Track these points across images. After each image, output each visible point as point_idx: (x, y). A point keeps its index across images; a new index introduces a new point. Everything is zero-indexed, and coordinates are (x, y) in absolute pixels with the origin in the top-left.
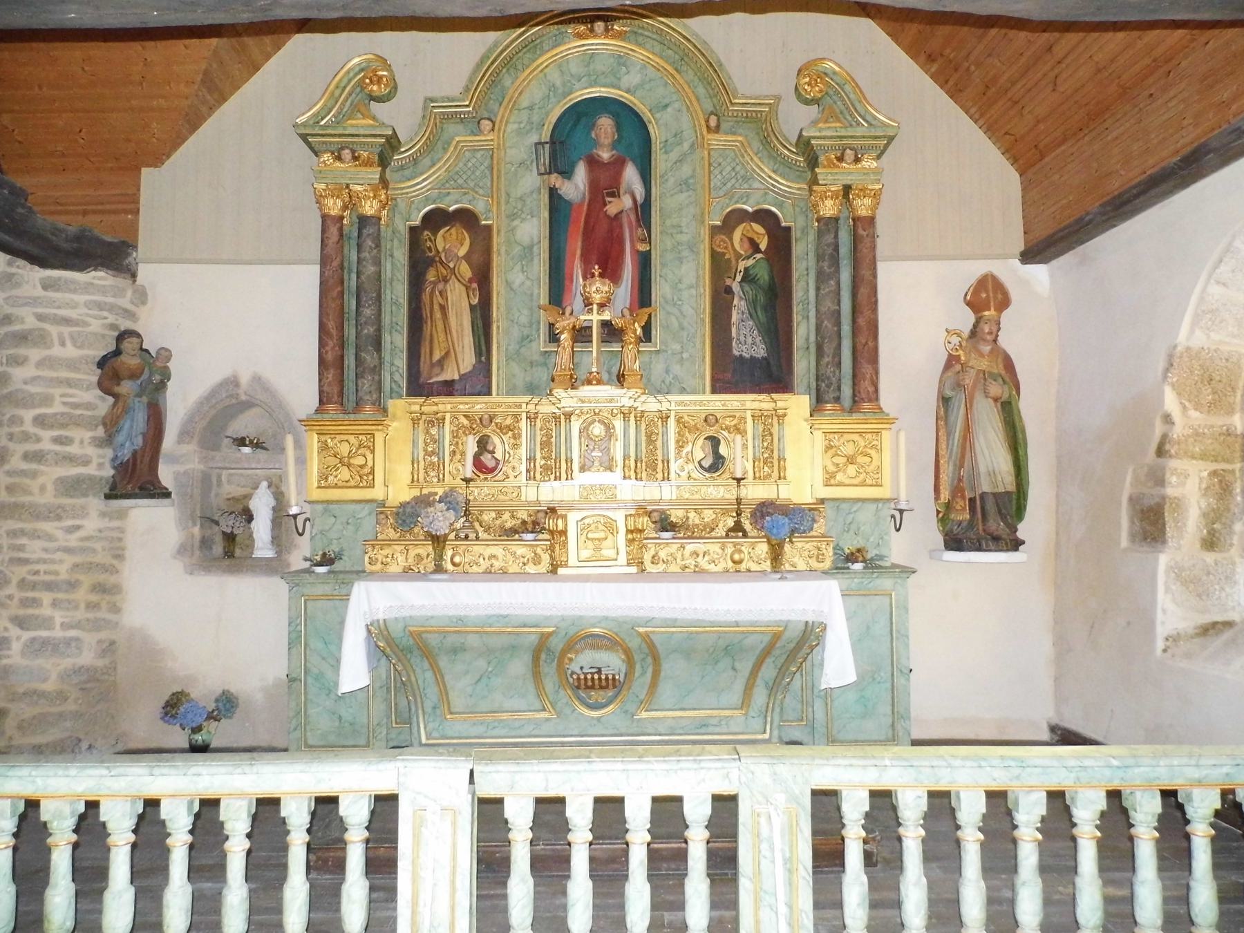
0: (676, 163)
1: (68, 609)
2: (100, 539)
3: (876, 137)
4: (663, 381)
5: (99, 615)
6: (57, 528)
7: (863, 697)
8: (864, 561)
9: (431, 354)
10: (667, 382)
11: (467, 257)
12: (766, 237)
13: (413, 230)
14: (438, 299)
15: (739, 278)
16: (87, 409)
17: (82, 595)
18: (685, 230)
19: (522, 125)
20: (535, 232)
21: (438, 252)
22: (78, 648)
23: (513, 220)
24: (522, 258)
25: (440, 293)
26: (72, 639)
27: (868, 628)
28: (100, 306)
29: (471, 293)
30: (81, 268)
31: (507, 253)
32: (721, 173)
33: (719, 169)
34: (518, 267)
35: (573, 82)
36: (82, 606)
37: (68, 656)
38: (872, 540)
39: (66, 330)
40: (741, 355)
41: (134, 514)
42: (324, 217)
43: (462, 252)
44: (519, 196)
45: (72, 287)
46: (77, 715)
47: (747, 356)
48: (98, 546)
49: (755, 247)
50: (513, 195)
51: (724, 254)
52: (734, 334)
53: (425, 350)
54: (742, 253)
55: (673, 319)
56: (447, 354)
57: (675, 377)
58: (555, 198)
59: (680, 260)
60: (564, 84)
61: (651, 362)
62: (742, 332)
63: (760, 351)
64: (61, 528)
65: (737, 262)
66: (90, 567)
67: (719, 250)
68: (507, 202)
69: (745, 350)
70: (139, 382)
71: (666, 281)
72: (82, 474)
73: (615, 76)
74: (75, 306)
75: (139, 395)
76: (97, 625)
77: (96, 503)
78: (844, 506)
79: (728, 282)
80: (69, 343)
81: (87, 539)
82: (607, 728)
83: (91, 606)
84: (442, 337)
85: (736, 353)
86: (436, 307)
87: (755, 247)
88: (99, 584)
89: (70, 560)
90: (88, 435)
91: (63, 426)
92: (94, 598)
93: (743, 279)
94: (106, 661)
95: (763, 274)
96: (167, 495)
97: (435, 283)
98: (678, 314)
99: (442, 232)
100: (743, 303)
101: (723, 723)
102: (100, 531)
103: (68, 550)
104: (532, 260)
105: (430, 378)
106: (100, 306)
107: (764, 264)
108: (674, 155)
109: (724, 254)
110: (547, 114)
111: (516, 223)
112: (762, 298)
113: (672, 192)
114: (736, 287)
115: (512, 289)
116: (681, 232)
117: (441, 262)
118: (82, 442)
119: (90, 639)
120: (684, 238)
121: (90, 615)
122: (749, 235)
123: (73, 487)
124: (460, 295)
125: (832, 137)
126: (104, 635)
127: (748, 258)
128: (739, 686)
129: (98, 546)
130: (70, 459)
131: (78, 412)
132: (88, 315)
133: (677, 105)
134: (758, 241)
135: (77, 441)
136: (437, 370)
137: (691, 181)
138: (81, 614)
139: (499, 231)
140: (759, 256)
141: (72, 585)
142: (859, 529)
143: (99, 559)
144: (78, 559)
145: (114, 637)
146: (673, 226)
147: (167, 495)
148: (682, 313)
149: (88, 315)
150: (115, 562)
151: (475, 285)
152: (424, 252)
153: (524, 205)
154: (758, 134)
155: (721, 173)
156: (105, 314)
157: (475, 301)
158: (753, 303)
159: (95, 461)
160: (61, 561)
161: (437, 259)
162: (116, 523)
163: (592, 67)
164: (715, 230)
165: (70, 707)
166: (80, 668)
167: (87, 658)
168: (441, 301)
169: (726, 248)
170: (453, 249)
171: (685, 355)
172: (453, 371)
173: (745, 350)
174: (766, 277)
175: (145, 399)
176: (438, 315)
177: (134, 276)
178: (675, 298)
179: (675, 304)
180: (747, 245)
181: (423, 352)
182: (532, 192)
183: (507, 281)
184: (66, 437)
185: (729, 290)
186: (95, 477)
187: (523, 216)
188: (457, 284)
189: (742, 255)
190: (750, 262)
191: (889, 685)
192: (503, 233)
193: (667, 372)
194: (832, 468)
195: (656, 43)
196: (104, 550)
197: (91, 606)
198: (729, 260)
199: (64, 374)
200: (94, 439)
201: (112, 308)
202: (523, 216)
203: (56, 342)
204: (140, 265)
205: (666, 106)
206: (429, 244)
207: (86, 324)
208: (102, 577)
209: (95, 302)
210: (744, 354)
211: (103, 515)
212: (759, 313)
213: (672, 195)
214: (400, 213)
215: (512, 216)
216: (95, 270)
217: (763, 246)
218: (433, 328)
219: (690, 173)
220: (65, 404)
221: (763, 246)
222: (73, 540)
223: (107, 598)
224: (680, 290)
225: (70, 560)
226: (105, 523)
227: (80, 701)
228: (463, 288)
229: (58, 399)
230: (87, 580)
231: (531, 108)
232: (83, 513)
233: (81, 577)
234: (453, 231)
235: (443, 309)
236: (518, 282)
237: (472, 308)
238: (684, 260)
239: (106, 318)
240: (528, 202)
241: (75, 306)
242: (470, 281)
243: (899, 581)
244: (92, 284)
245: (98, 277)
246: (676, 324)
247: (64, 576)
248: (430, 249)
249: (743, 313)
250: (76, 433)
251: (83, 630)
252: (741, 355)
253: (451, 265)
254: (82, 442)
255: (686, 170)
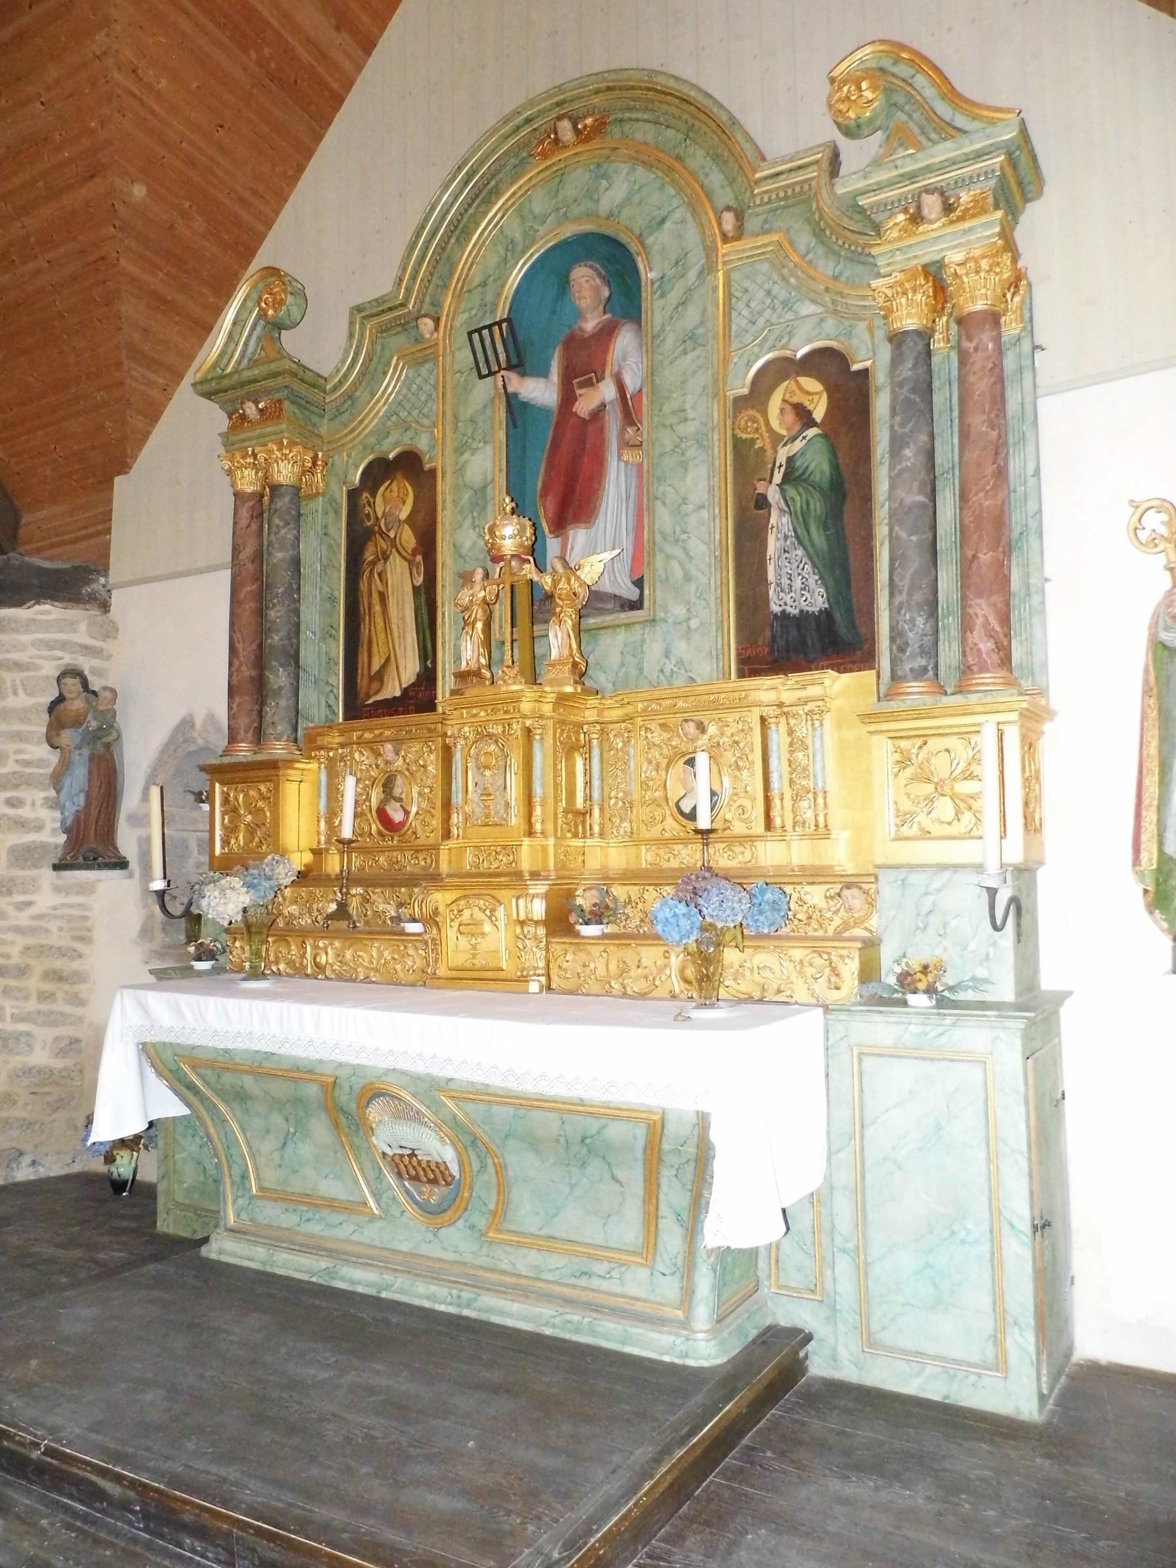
0: (677, 307)
1: (17, 999)
2: (55, 917)
3: (979, 155)
4: (662, 671)
5: (53, 1007)
6: (8, 904)
7: (929, 1266)
8: (930, 990)
9: (370, 662)
10: (667, 672)
11: (410, 520)
12: (825, 396)
13: (353, 495)
14: (377, 584)
15: (778, 477)
16: (38, 766)
17: (33, 983)
18: (691, 415)
19: (474, 312)
20: (489, 465)
21: (377, 519)
22: (28, 1045)
23: (462, 453)
24: (473, 505)
25: (379, 575)
26: (21, 1033)
27: (939, 1128)
28: (48, 645)
29: (415, 570)
30: (19, 604)
31: (455, 503)
32: (748, 306)
33: (746, 298)
34: (468, 522)
35: (536, 227)
36: (34, 996)
37: (17, 1054)
38: (972, 946)
39: (19, 676)
40: (784, 611)
41: (101, 888)
42: (238, 496)
43: (404, 513)
44: (469, 416)
45: (13, 625)
46: (27, 1124)
47: (795, 612)
48: (53, 926)
49: (804, 416)
50: (462, 417)
51: (753, 441)
52: (771, 576)
53: (363, 658)
54: (784, 432)
55: (675, 565)
56: (388, 660)
57: (680, 663)
58: (516, 409)
59: (684, 466)
60: (525, 234)
61: (643, 641)
62: (785, 570)
63: (816, 600)
64: (13, 904)
65: (776, 452)
66: (42, 951)
67: (744, 436)
68: (456, 429)
69: (789, 602)
70: (80, 730)
71: (664, 504)
72: (34, 842)
73: (591, 199)
74: (23, 648)
75: (78, 747)
76: (53, 1020)
77: (47, 876)
78: (916, 878)
79: (761, 487)
80: (20, 691)
81: (41, 917)
82: (444, 1249)
83: (44, 997)
84: (382, 636)
85: (775, 608)
86: (375, 596)
87: (804, 416)
88: (55, 972)
89: (22, 941)
90: (40, 795)
91: (16, 787)
92: (48, 987)
93: (786, 479)
94: (69, 1062)
95: (819, 464)
96: (122, 864)
97: (373, 563)
98: (683, 556)
99: (382, 489)
100: (785, 519)
101: (615, 1274)
102: (55, 908)
103: (17, 930)
104: (485, 508)
105: (369, 697)
106: (48, 645)
107: (821, 444)
108: (674, 297)
109: (753, 441)
110: (503, 286)
111: (466, 456)
112: (817, 506)
113: (671, 358)
114: (773, 494)
115: (461, 556)
116: (686, 420)
117: (381, 533)
118: (33, 804)
119: (45, 1034)
120: (690, 428)
121: (44, 1007)
122: (795, 400)
123: (24, 856)
124: (402, 574)
125: (891, 184)
126: (65, 1031)
127: (794, 439)
128: (633, 1211)
129: (53, 926)
130: (21, 825)
131: (28, 770)
132: (41, 657)
133: (677, 215)
134: (810, 408)
135: (29, 803)
136: (375, 686)
137: (701, 331)
138: (32, 1005)
139: (443, 473)
140: (812, 432)
141: (22, 972)
142: (945, 925)
143: (55, 940)
144: (31, 941)
145: (77, 1034)
146: (674, 413)
147: (122, 864)
148: (687, 554)
149: (41, 657)
150: (77, 945)
151: (419, 558)
152: (362, 521)
153: (475, 430)
154: (808, 220)
155: (748, 306)
156: (59, 653)
157: (419, 581)
158: (802, 519)
159: (49, 826)
160: (13, 943)
161: (376, 528)
162: (80, 899)
163: (560, 197)
164: (740, 403)
165: (18, 1113)
166: (30, 1070)
167: (40, 1057)
168: (381, 589)
169: (757, 430)
170: (394, 511)
171: (694, 623)
172: (394, 685)
173: (789, 602)
174: (826, 467)
175: (86, 752)
176: (377, 608)
177: (105, 607)
178: (678, 530)
179: (677, 541)
180: (790, 417)
181: (360, 662)
182: (486, 406)
183: (454, 545)
184: (17, 799)
185: (762, 502)
186: (49, 844)
187: (474, 445)
188: (398, 560)
189: (783, 437)
190: (798, 445)
191: (985, 1249)
192: (448, 475)
193: (667, 654)
194: (906, 805)
195: (648, 126)
196: (61, 929)
197: (44, 997)
198: (762, 450)
199: (16, 727)
200: (46, 799)
201: (63, 645)
202: (474, 445)
203: (10, 691)
204: (114, 593)
205: (663, 221)
206: (367, 509)
207: (37, 668)
208: (59, 964)
209: (41, 641)
210: (789, 609)
211: (57, 889)
212: (813, 529)
213: (671, 363)
214: (337, 475)
215: (460, 450)
216: (38, 603)
217: (819, 415)
218: (372, 628)
219: (697, 319)
220: (17, 761)
221: (819, 415)
222: (23, 919)
223: (67, 987)
224: (687, 515)
225: (22, 941)
226: (60, 899)
227: (30, 1107)
228: (406, 564)
229: (12, 757)
230: (38, 966)
231: (484, 284)
232: (31, 886)
233: (33, 962)
234: (394, 486)
235: (383, 597)
236: (468, 544)
237: (416, 590)
238: (691, 464)
239: (62, 658)
240: (480, 424)
241: (23, 648)
242: (415, 552)
243: (1002, 1035)
244: (34, 620)
245: (46, 612)
246: (679, 574)
247: (15, 959)
248: (368, 515)
249: (786, 537)
250: (27, 794)
251: (36, 1023)
252: (784, 611)
253: (392, 534)
254: (33, 804)
255: (692, 315)
